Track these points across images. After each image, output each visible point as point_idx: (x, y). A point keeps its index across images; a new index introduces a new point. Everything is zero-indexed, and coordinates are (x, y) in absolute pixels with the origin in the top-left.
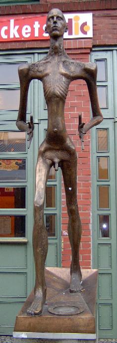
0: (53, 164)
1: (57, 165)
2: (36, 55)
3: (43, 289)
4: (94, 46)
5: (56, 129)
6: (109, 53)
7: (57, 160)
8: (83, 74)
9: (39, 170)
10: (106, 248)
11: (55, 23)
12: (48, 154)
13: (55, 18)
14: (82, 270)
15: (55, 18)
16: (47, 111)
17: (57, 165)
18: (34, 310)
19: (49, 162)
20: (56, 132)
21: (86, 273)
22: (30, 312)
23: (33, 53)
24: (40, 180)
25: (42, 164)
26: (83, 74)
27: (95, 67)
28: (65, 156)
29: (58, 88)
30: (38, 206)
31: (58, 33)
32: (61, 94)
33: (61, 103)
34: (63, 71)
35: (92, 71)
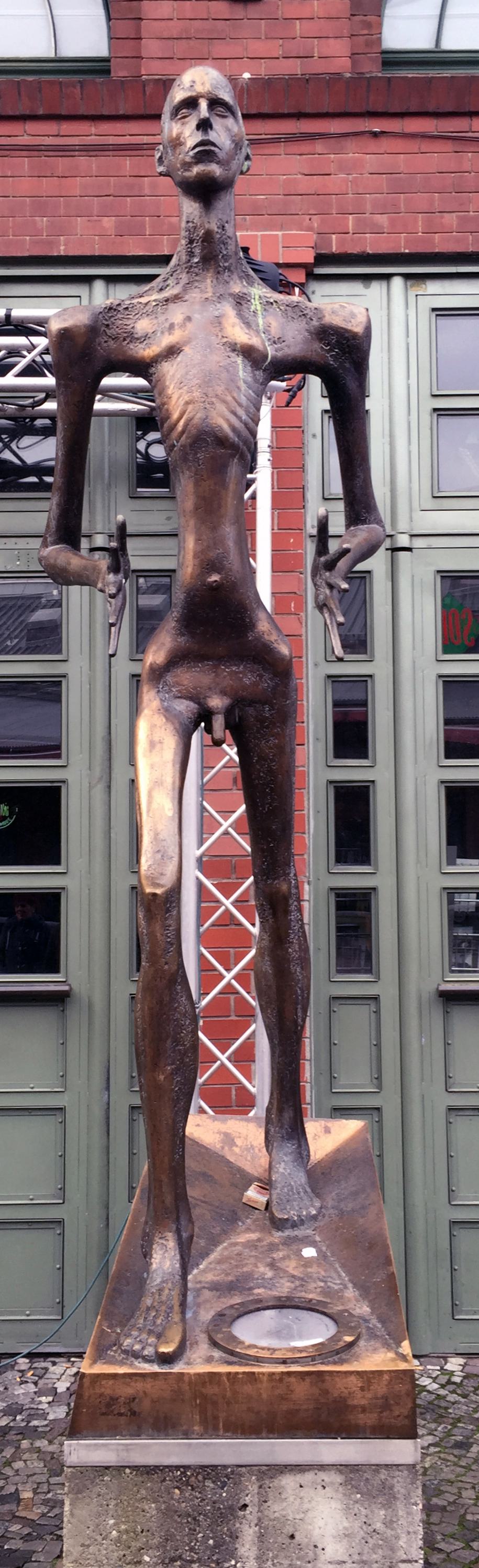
0: (204, 716)
1: (218, 723)
2: (99, 286)
3: (178, 1232)
4: (322, 259)
5: (215, 578)
6: (377, 288)
7: (216, 702)
8: (317, 349)
9: (152, 745)
10: (363, 1012)
11: (205, 125)
12: (187, 677)
13: (203, 104)
14: (312, 1127)
15: (203, 104)
16: (367, 408)
17: (218, 723)
18: (152, 1340)
19: (184, 707)
20: (215, 589)
21: (327, 1137)
22: (137, 1347)
23: (88, 280)
24: (157, 783)
25: (160, 720)
26: (317, 349)
27: (362, 319)
28: (247, 677)
29: (222, 408)
30: (159, 891)
31: (215, 169)
32: (234, 429)
33: (234, 469)
34: (241, 336)
35: (355, 336)
